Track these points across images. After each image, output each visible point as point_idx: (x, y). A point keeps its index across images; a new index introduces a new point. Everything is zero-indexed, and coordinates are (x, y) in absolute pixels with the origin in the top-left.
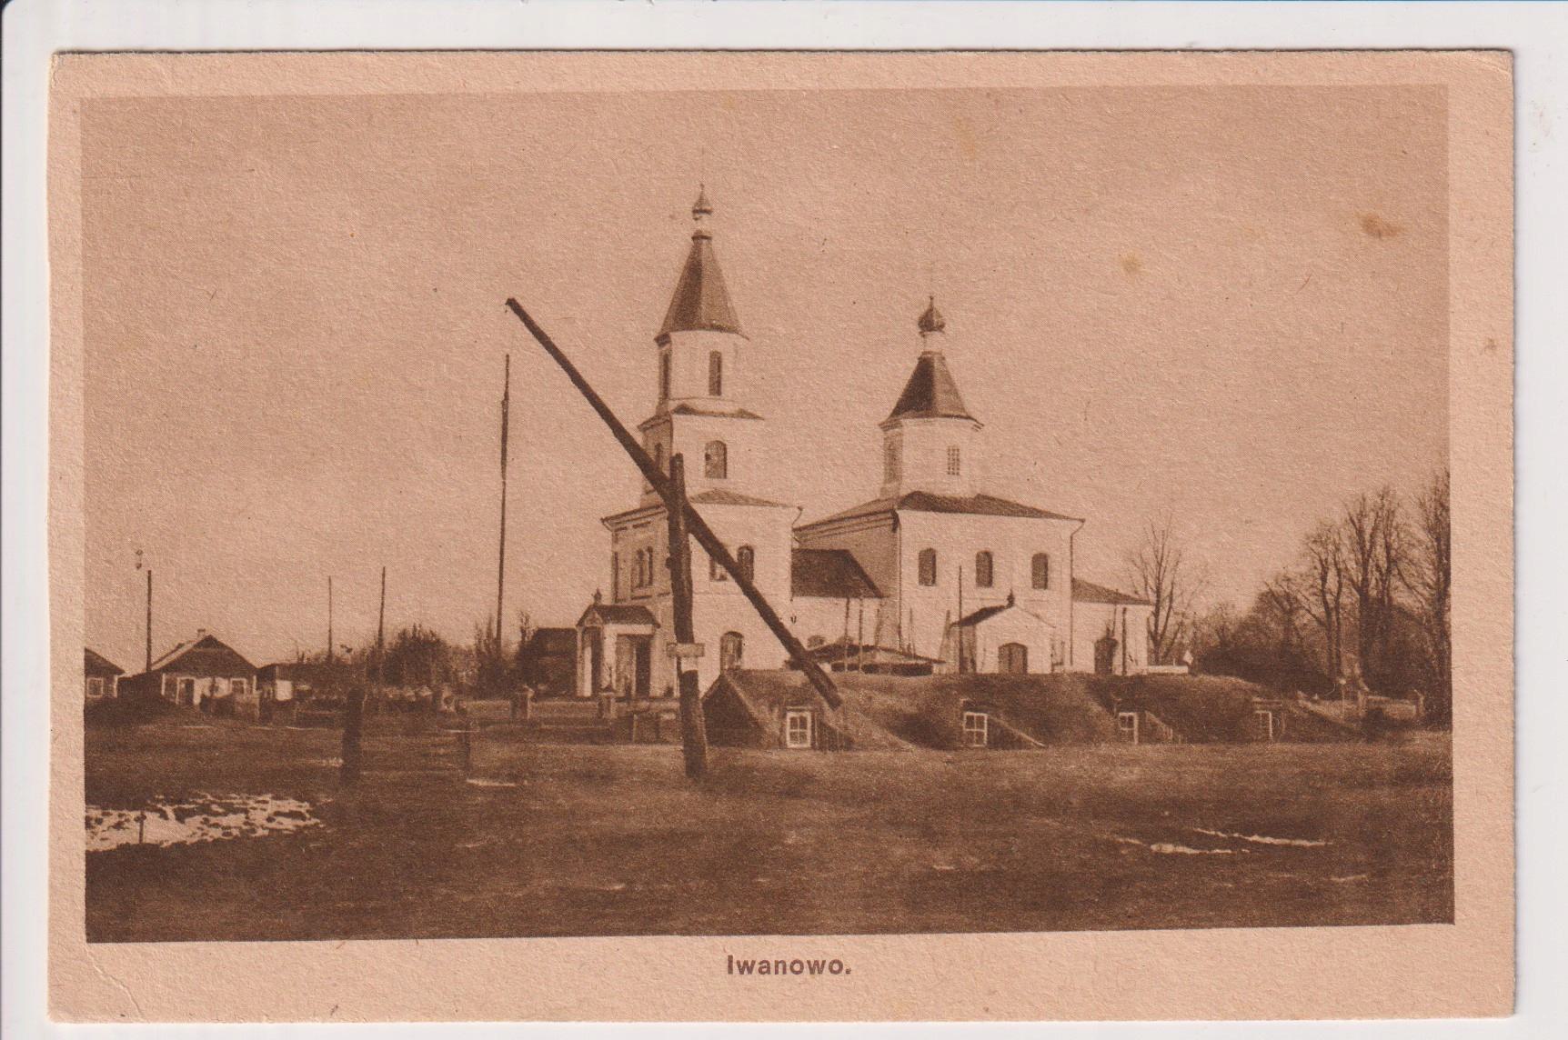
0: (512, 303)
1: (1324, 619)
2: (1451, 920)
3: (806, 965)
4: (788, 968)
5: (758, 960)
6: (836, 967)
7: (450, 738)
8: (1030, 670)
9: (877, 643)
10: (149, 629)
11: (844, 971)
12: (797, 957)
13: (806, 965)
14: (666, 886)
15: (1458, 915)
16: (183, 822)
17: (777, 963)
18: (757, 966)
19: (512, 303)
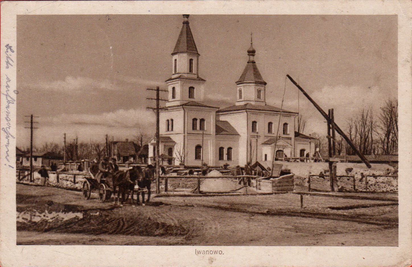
0: (288, 76)
1: (383, 140)
2: (18, 16)
3: (213, 251)
4: (209, 253)
5: (202, 251)
6: (220, 252)
7: (392, 143)
8: (182, 112)
9: (161, 109)
10: (172, 101)
11: (222, 254)
12: (220, 255)
13: (213, 251)
14: (112, 55)
15: (15, 18)
16: (126, 139)
17: (207, 251)
18: (202, 252)
19: (288, 76)
